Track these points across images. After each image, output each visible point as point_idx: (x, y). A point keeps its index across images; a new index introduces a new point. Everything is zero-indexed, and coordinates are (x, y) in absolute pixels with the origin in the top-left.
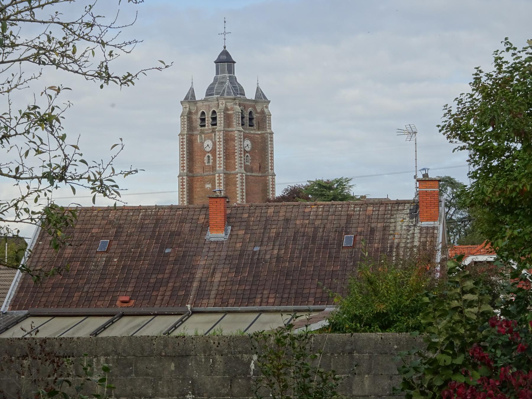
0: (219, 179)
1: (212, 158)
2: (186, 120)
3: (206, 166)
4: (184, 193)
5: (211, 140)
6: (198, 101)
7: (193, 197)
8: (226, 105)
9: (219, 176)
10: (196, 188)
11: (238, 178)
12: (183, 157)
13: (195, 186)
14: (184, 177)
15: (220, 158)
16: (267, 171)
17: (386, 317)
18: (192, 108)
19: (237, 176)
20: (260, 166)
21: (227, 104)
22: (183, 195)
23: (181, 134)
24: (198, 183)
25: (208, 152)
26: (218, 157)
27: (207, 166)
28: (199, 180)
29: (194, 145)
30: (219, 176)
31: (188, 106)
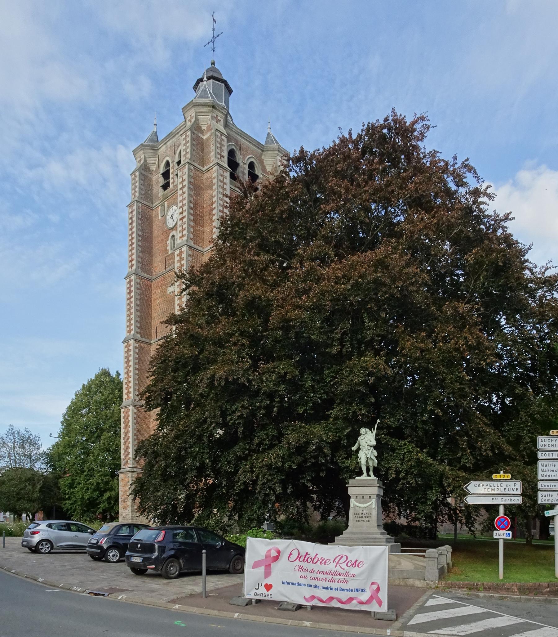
8: (196, 118)
18: (150, 160)
23: (130, 206)
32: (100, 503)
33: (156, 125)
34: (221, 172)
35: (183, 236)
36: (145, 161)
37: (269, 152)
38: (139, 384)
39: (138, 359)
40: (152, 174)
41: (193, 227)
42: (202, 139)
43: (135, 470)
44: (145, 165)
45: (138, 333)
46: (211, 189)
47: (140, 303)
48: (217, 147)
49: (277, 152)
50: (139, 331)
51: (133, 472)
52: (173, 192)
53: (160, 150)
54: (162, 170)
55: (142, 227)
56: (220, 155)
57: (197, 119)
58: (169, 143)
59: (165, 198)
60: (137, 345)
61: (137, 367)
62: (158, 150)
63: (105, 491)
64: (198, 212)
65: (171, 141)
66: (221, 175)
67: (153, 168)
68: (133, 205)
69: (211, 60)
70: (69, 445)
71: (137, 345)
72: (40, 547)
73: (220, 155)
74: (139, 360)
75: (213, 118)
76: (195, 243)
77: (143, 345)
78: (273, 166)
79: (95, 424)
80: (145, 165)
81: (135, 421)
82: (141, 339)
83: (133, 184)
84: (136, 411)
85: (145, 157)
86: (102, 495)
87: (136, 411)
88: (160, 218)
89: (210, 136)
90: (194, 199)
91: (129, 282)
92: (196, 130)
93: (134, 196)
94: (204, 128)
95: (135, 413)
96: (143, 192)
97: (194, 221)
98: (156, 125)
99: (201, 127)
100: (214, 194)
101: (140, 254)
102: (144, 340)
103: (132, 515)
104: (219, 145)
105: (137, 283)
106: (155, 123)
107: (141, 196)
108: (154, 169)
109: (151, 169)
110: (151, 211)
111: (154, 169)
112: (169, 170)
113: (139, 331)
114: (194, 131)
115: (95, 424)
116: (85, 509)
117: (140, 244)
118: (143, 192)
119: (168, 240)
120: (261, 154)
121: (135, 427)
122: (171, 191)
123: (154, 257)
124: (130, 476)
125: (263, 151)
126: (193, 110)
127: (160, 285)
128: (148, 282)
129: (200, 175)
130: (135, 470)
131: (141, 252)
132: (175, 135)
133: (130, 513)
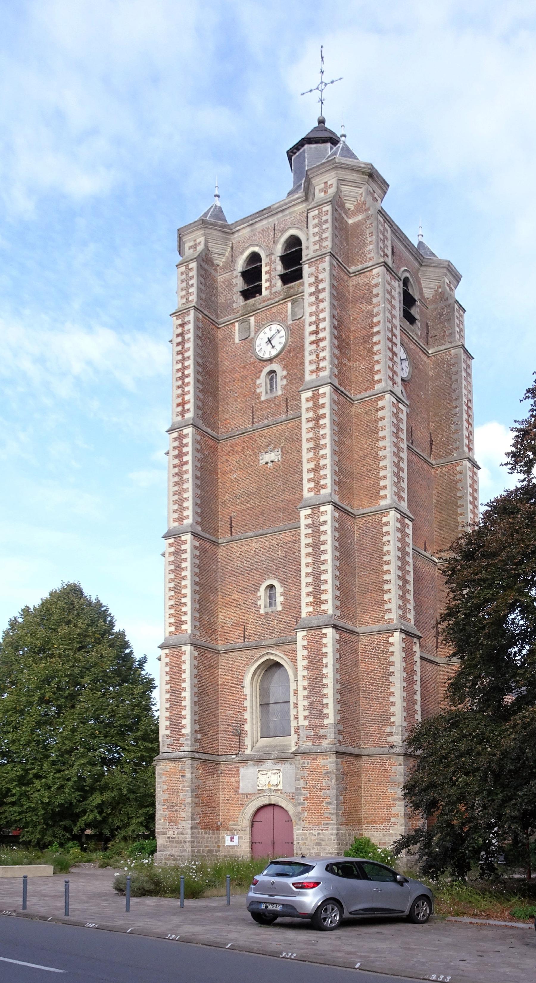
0: (317, 406)
1: (285, 373)
2: (194, 273)
3: (261, 403)
4: (185, 477)
5: (283, 322)
6: (237, 224)
7: (216, 497)
8: (338, 188)
9: (315, 397)
10: (225, 473)
11: (382, 408)
12: (182, 378)
13: (221, 467)
14: (185, 431)
15: (316, 342)
16: (458, 448)
17: (456, 873)
18: (215, 248)
19: (380, 404)
20: (431, 441)
21: (343, 188)
22: (182, 509)
23: (178, 314)
24: (233, 459)
25: (270, 360)
26: (312, 343)
27: (267, 401)
28: (238, 448)
29: (222, 355)
30: (315, 397)
31: (202, 240)
32: (84, 812)
33: (218, 196)
34: (388, 277)
35: (318, 369)
36: (206, 247)
37: (431, 269)
38: (200, 609)
39: (199, 566)
40: (216, 270)
41: (337, 358)
42: (347, 222)
43: (197, 755)
44: (206, 255)
45: (198, 523)
46: (370, 302)
47: (202, 475)
48: (378, 239)
49: (445, 271)
50: (199, 520)
51: (193, 759)
52: (269, 302)
53: (236, 235)
54: (240, 264)
55: (203, 352)
56: (384, 252)
57: (339, 190)
58: (259, 225)
59: (248, 312)
60: (197, 544)
61: (197, 580)
62: (233, 233)
63: (93, 790)
64: (344, 336)
65: (264, 222)
66: (389, 283)
67: (221, 261)
68: (187, 314)
69: (318, 115)
70: (15, 708)
71: (197, 544)
72: (323, 915)
73: (384, 252)
74: (200, 569)
75: (368, 193)
76: (340, 384)
77: (207, 545)
78: (436, 291)
79: (67, 676)
80: (206, 255)
81: (196, 672)
82: (202, 534)
83: (182, 281)
84: (196, 654)
85: (206, 242)
86: (85, 798)
87: (196, 654)
88: (237, 341)
89: (364, 220)
90: (338, 314)
91: (180, 438)
92: (339, 206)
93: (184, 301)
94: (349, 206)
95: (195, 658)
96: (203, 296)
97: (339, 347)
98: (218, 196)
99: (344, 204)
100: (375, 310)
101: (201, 395)
102: (208, 536)
103: (192, 833)
104: (381, 236)
105: (195, 441)
106: (217, 193)
107: (201, 302)
108: (221, 264)
109: (215, 262)
110: (215, 329)
111: (221, 264)
112: (259, 269)
113: (199, 520)
114: (337, 207)
115: (67, 676)
116: (50, 822)
117: (200, 378)
118: (203, 296)
119: (258, 378)
120: (418, 270)
121: (196, 681)
122: (264, 301)
123: (221, 403)
124: (189, 766)
125: (421, 265)
126: (333, 173)
127: (238, 448)
128: (212, 443)
129: (346, 277)
130: (197, 755)
131: (201, 391)
132: (277, 213)
133: (189, 831)
